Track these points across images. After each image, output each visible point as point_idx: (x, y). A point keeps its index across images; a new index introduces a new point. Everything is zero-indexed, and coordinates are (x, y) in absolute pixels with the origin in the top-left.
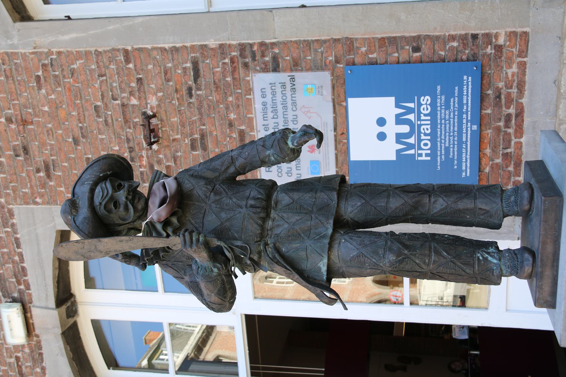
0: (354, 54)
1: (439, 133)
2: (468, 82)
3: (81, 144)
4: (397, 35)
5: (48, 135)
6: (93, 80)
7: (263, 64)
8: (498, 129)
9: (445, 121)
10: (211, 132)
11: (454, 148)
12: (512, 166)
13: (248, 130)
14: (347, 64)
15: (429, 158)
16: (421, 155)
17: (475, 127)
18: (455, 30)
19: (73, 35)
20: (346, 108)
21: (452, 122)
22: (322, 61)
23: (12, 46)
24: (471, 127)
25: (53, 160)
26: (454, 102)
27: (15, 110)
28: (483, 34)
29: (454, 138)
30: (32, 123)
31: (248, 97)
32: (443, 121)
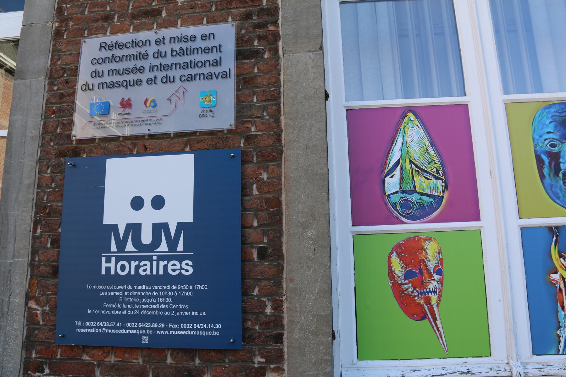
0: (258, 162)
1: (139, 287)
2: (211, 330)
4: (284, 224)
7: (249, 38)
9: (156, 297)
11: (117, 309)
14: (243, 153)
15: (103, 272)
16: (108, 260)
17: (145, 340)
18: (288, 309)
20: (181, 151)
21: (154, 306)
22: (250, 117)
24: (145, 335)
26: (183, 310)
28: (282, 350)
29: (131, 309)
31: (205, 19)
32: (156, 294)
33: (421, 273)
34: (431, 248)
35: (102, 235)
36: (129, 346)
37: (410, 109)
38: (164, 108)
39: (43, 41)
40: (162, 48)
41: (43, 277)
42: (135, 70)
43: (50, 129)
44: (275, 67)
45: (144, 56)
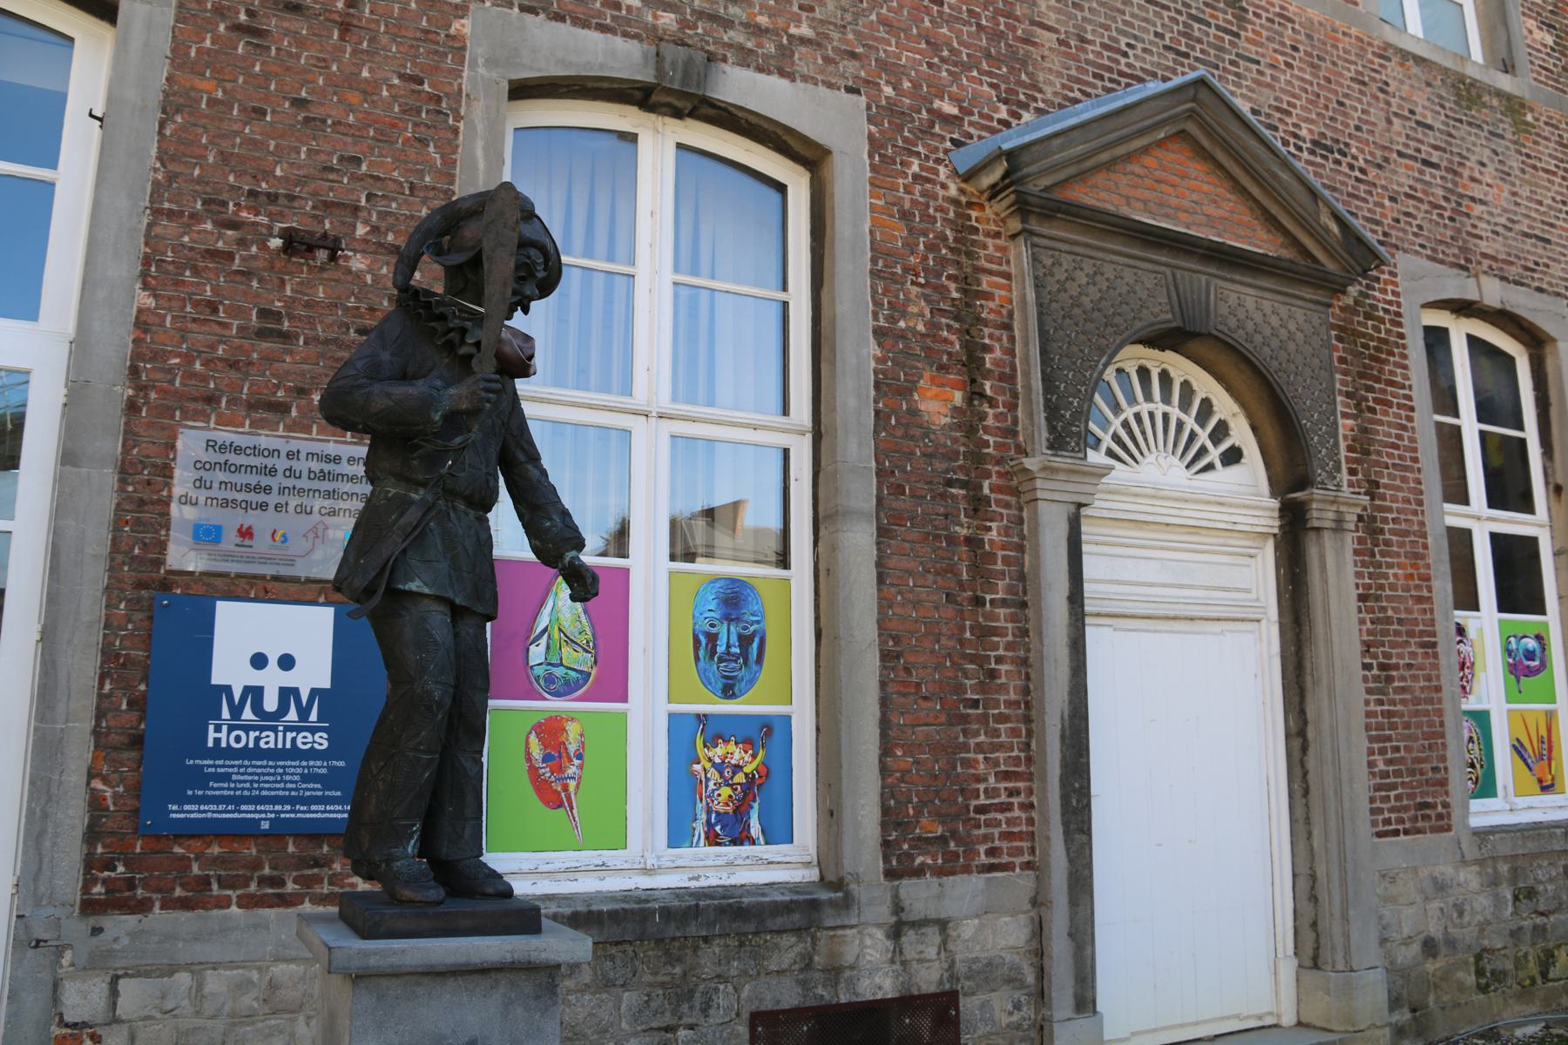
3: (293, 110)
5: (318, 59)
6: (407, 171)
8: (257, 865)
10: (291, 353)
11: (229, 789)
12: (184, 894)
13: (288, 421)
15: (210, 744)
16: (218, 729)
17: (265, 826)
19: (481, 165)
25: (268, 48)
27: (369, 21)
30: (342, 38)
33: (560, 757)
34: (573, 730)
40: (297, 466)
41: (115, 748)
42: (257, 489)
43: (124, 548)
45: (272, 472)
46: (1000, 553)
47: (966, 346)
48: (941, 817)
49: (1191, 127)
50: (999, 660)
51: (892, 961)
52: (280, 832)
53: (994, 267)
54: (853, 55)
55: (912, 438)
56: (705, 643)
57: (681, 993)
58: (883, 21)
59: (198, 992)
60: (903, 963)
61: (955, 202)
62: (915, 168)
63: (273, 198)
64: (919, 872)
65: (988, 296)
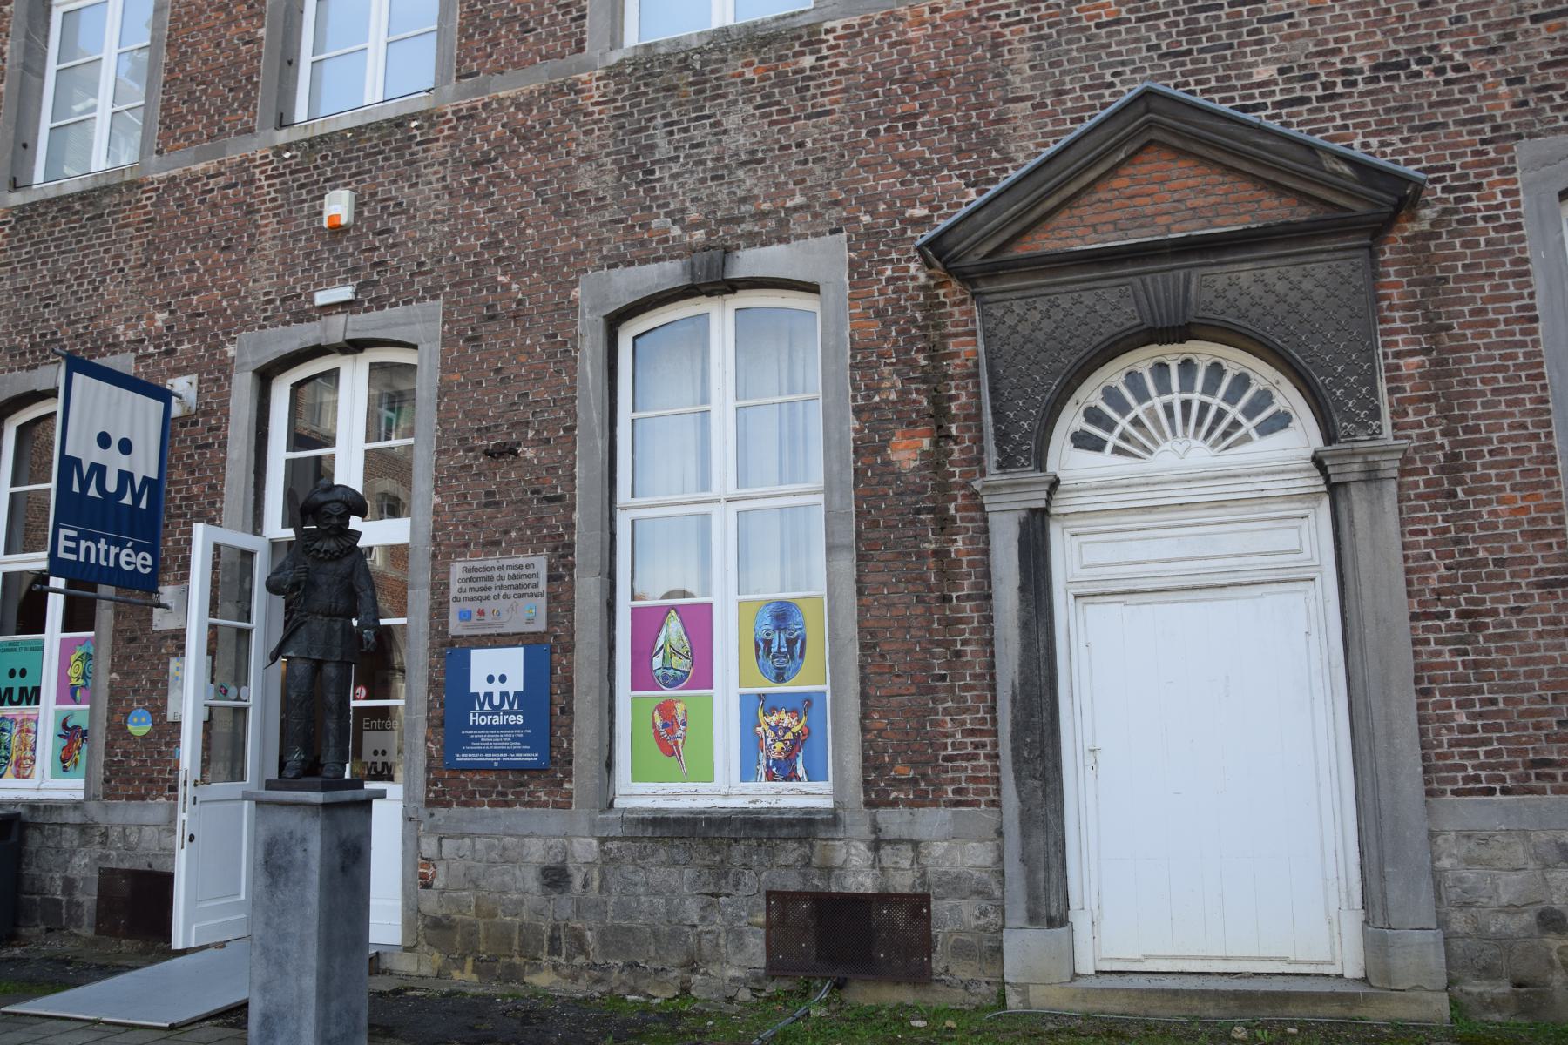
8: (495, 786)
19: (590, 376)
23: (583, 313)
34: (680, 708)
35: (469, 700)
36: (486, 768)
37: (673, 607)
38: (505, 617)
39: (425, 548)
44: (572, 588)
45: (490, 579)
46: (965, 559)
47: (932, 401)
48: (912, 764)
49: (1156, 135)
50: (965, 642)
51: (873, 867)
52: (503, 769)
53: (960, 329)
54: (836, 203)
55: (886, 483)
56: (763, 647)
57: (720, 872)
58: (864, 165)
59: (473, 848)
60: (882, 869)
61: (924, 288)
62: (889, 273)
63: (488, 429)
64: (894, 804)
65: (955, 355)
